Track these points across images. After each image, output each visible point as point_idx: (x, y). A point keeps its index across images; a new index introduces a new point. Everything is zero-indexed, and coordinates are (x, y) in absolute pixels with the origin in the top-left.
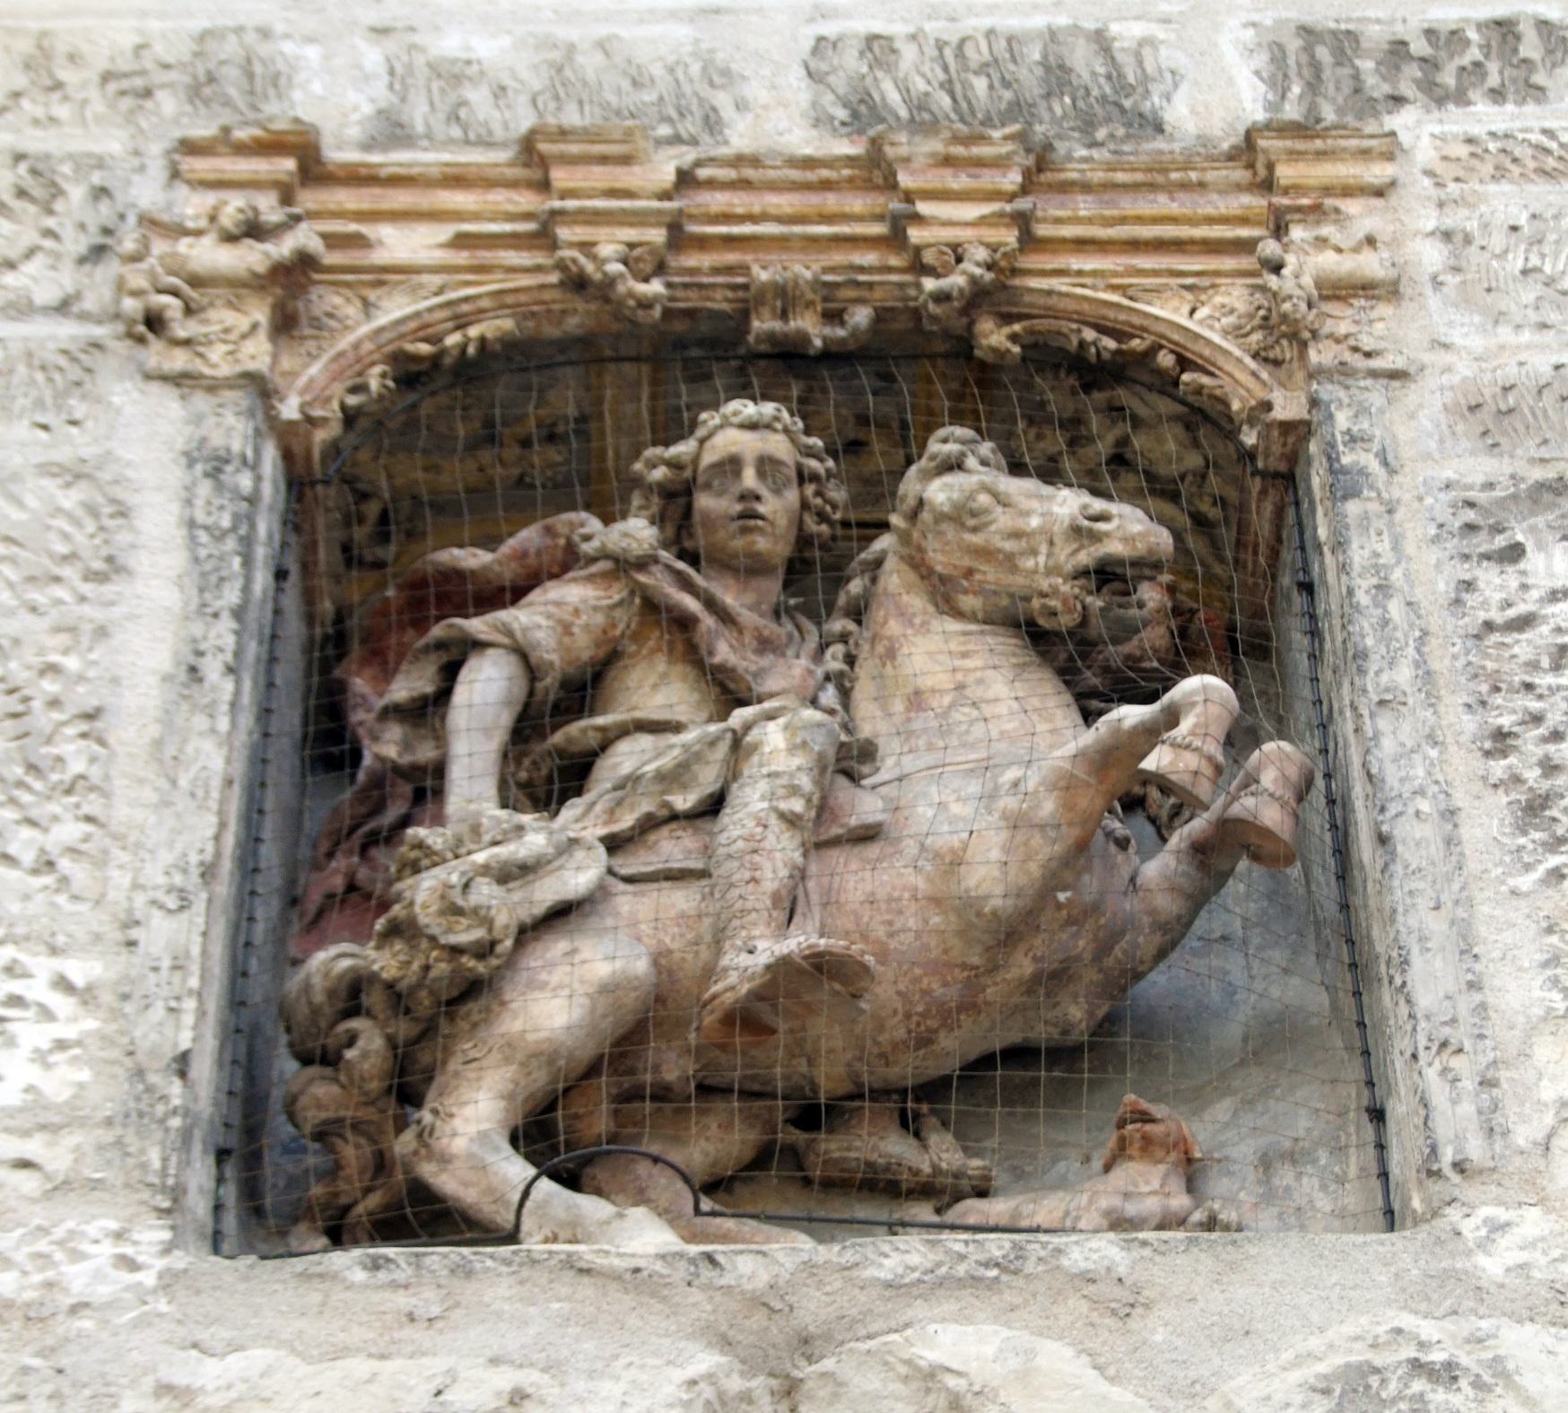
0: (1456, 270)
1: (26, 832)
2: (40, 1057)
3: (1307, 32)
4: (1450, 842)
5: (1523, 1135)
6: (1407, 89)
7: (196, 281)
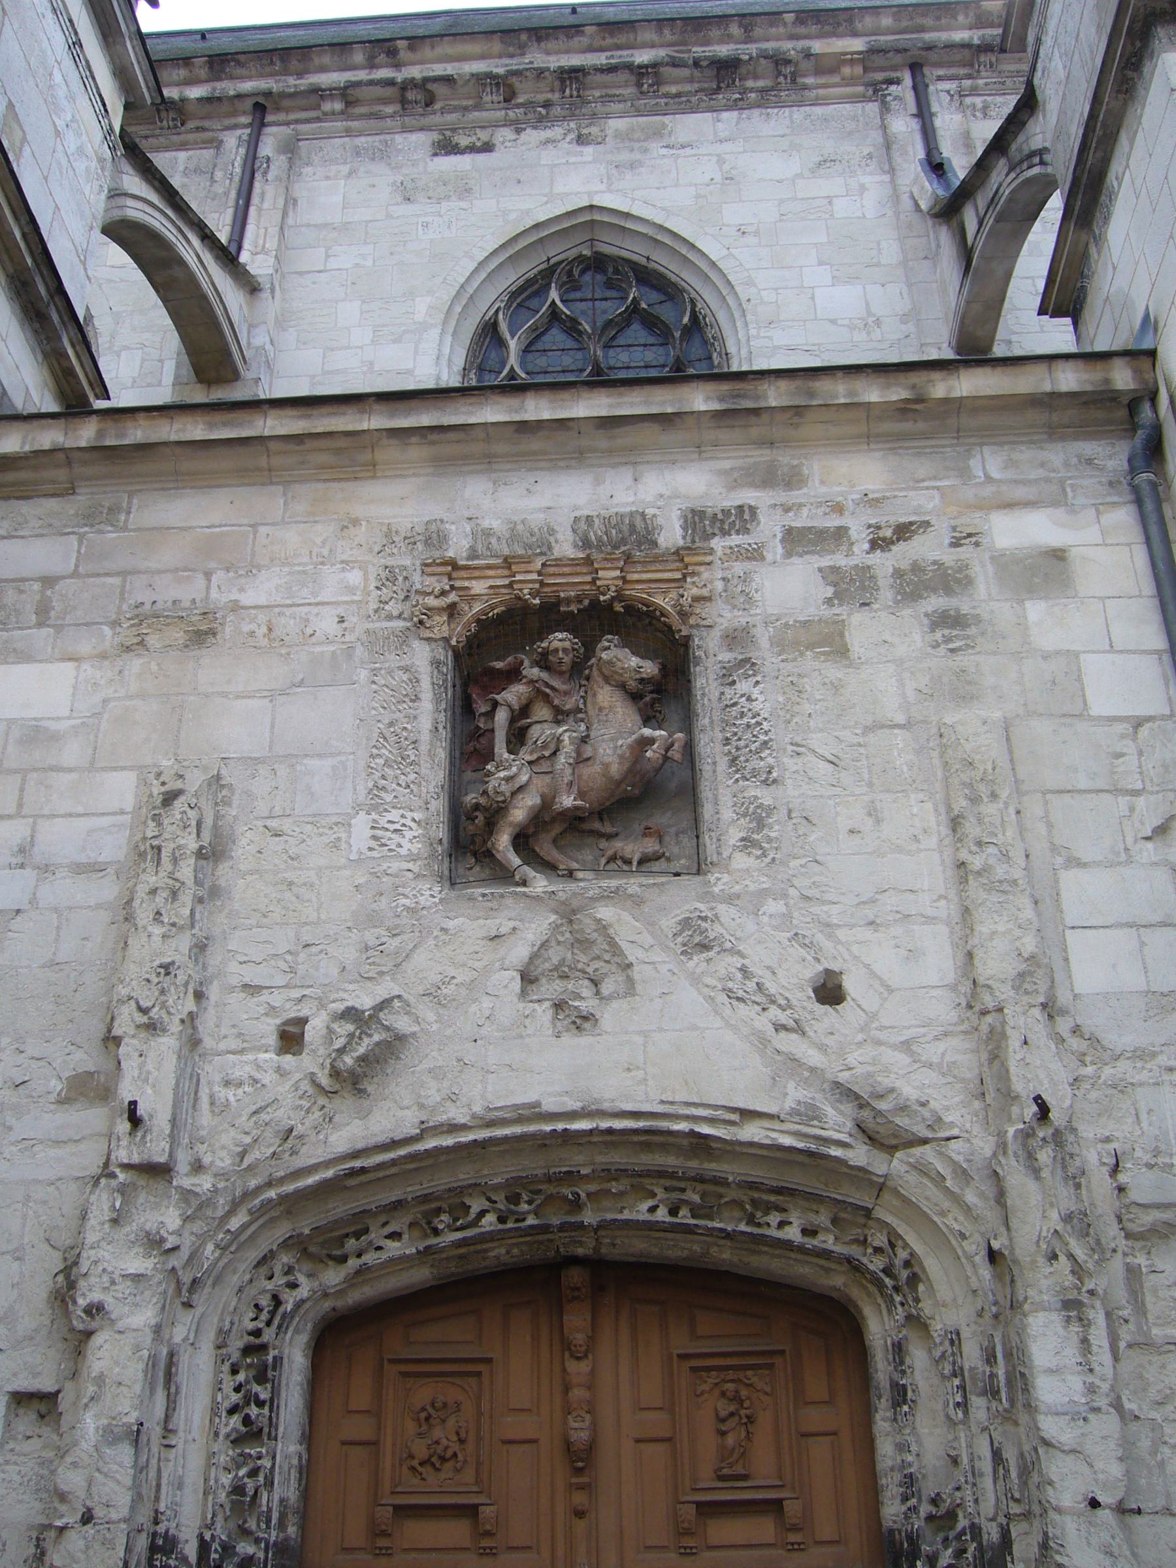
0: (725, 591)
1: (403, 777)
2: (410, 841)
3: (693, 511)
4: (714, 771)
5: (725, 854)
6: (717, 531)
7: (429, 609)
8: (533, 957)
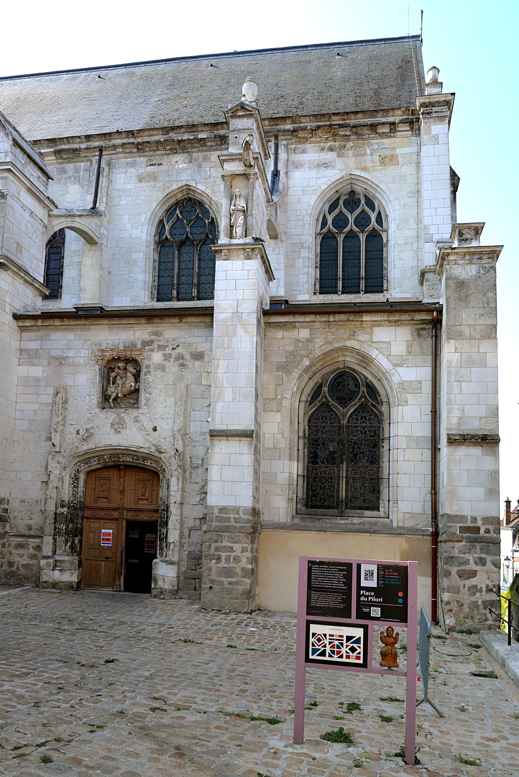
8: (112, 422)
